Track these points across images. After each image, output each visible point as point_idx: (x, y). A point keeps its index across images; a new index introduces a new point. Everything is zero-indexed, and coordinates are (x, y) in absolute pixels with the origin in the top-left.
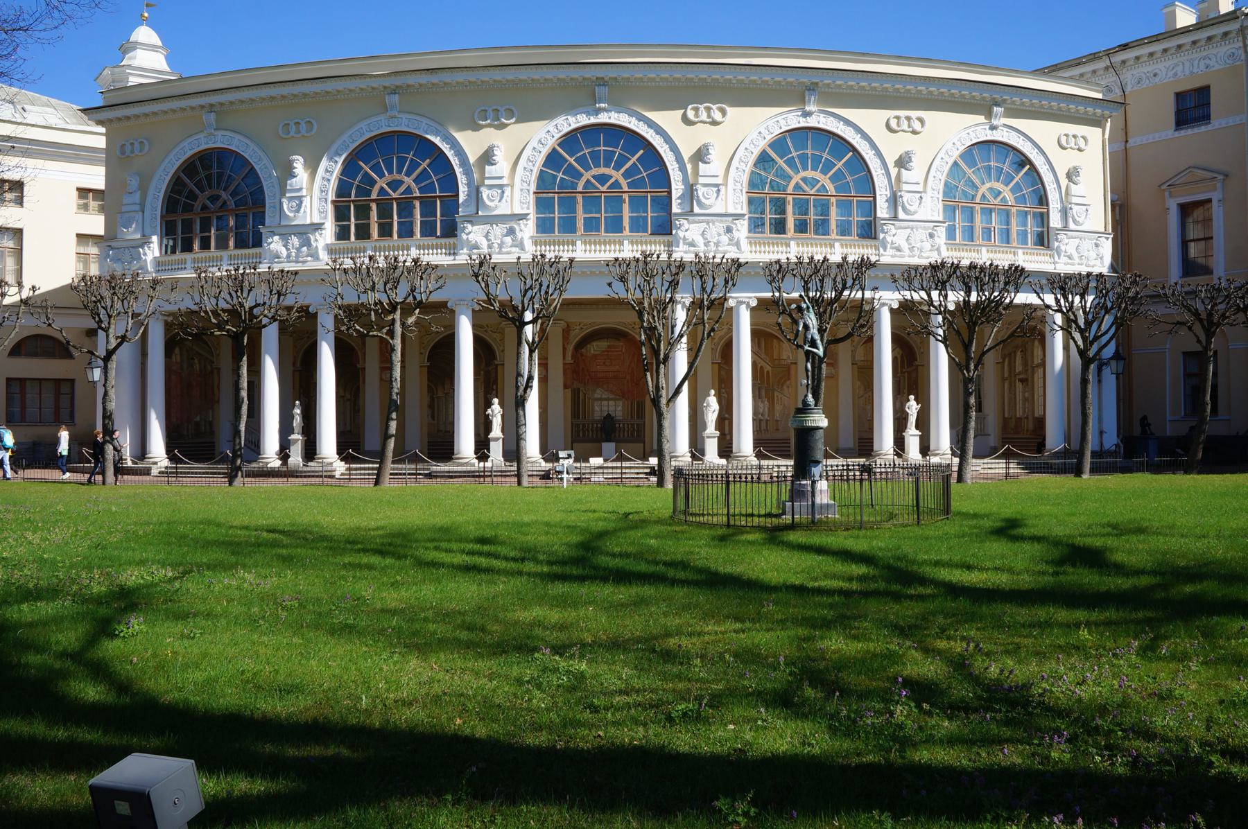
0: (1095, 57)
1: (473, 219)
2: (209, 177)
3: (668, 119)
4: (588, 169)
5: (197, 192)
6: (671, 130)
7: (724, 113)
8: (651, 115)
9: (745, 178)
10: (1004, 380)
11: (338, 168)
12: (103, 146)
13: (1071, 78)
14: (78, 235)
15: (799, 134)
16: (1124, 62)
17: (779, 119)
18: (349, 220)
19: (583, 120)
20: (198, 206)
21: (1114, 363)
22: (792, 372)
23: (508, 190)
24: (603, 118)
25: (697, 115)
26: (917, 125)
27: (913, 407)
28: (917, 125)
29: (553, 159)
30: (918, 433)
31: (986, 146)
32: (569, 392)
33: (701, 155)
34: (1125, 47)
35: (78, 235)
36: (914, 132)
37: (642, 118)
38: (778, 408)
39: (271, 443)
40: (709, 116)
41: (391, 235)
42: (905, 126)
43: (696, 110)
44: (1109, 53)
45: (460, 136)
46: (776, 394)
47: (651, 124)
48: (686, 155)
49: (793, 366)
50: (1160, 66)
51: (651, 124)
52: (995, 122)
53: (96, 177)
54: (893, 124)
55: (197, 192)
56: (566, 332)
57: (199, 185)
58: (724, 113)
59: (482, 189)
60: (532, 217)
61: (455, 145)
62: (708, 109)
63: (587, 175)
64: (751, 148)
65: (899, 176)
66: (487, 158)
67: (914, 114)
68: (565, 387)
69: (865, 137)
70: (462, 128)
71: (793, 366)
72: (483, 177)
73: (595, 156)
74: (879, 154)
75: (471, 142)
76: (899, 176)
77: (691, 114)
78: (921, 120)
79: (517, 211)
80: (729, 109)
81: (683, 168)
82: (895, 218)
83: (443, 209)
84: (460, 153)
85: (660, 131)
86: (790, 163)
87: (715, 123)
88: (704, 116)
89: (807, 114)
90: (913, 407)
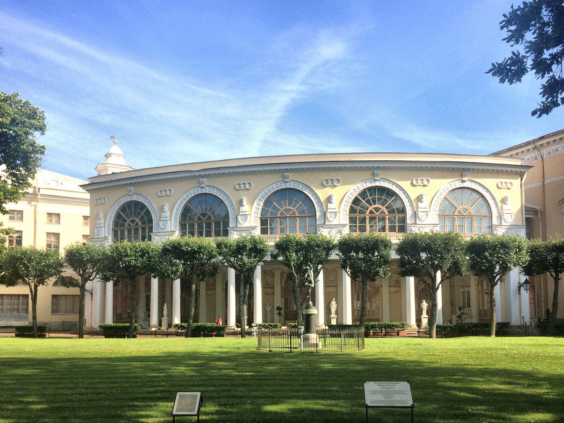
0: (528, 143)
1: (323, 225)
2: (139, 213)
3: (406, 185)
4: (371, 205)
5: (126, 219)
6: (406, 188)
7: (428, 181)
8: (399, 183)
9: (348, 209)
10: (479, 293)
11: (262, 204)
12: (89, 198)
13: (507, 157)
14: (83, 235)
15: (370, 189)
16: (542, 145)
17: (452, 183)
18: (203, 228)
19: (369, 185)
20: (126, 225)
21: (525, 285)
22: (380, 290)
23: (249, 216)
24: (378, 184)
25: (417, 183)
26: (509, 186)
27: (425, 305)
28: (509, 186)
29: (356, 201)
30: (427, 316)
31: (460, 191)
32: (283, 299)
33: (420, 199)
34: (542, 138)
35: (83, 235)
36: (508, 189)
37: (394, 183)
38: (374, 305)
39: (154, 320)
40: (422, 183)
41: (267, 234)
42: (504, 186)
43: (417, 180)
44: (534, 141)
45: (318, 192)
46: (373, 299)
47: (398, 186)
48: (498, 200)
49: (380, 288)
50: (559, 146)
51: (398, 186)
52: (464, 179)
53: (86, 211)
54: (500, 185)
55: (126, 219)
56: (282, 274)
57: (127, 216)
58: (428, 181)
59: (327, 213)
60: (348, 226)
61: (315, 194)
62: (422, 180)
63: (371, 208)
64: (440, 196)
65: (502, 207)
66: (329, 200)
67: (508, 181)
68: (282, 297)
69: (488, 191)
70: (318, 188)
71: (380, 288)
72: (327, 208)
73: (379, 199)
74: (493, 198)
75: (322, 193)
76: (502, 207)
77: (414, 182)
78: (511, 183)
79: (253, 225)
80: (431, 180)
81: (411, 205)
82: (416, 223)
83: (222, 225)
84: (317, 197)
85: (402, 189)
86: (368, 202)
87: (425, 186)
88: (420, 183)
89: (463, 181)
90: (425, 305)
